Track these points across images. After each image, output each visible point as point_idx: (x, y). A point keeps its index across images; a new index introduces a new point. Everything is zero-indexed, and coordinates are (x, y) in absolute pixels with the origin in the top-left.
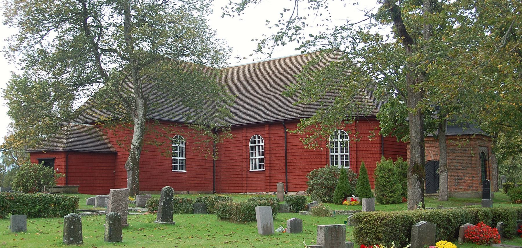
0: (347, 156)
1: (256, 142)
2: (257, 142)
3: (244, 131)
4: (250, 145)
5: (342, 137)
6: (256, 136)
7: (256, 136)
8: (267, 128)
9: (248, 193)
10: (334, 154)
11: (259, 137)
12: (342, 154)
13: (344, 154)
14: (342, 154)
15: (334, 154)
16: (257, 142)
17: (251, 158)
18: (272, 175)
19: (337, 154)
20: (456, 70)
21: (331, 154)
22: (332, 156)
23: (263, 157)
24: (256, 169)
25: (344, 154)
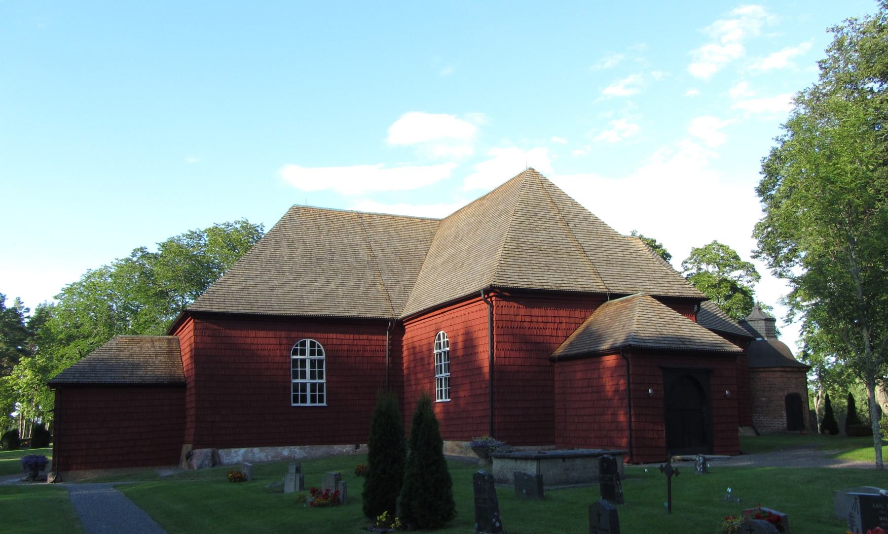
0: (321, 385)
1: (309, 353)
7: (308, 342)
10: (299, 381)
15: (299, 381)
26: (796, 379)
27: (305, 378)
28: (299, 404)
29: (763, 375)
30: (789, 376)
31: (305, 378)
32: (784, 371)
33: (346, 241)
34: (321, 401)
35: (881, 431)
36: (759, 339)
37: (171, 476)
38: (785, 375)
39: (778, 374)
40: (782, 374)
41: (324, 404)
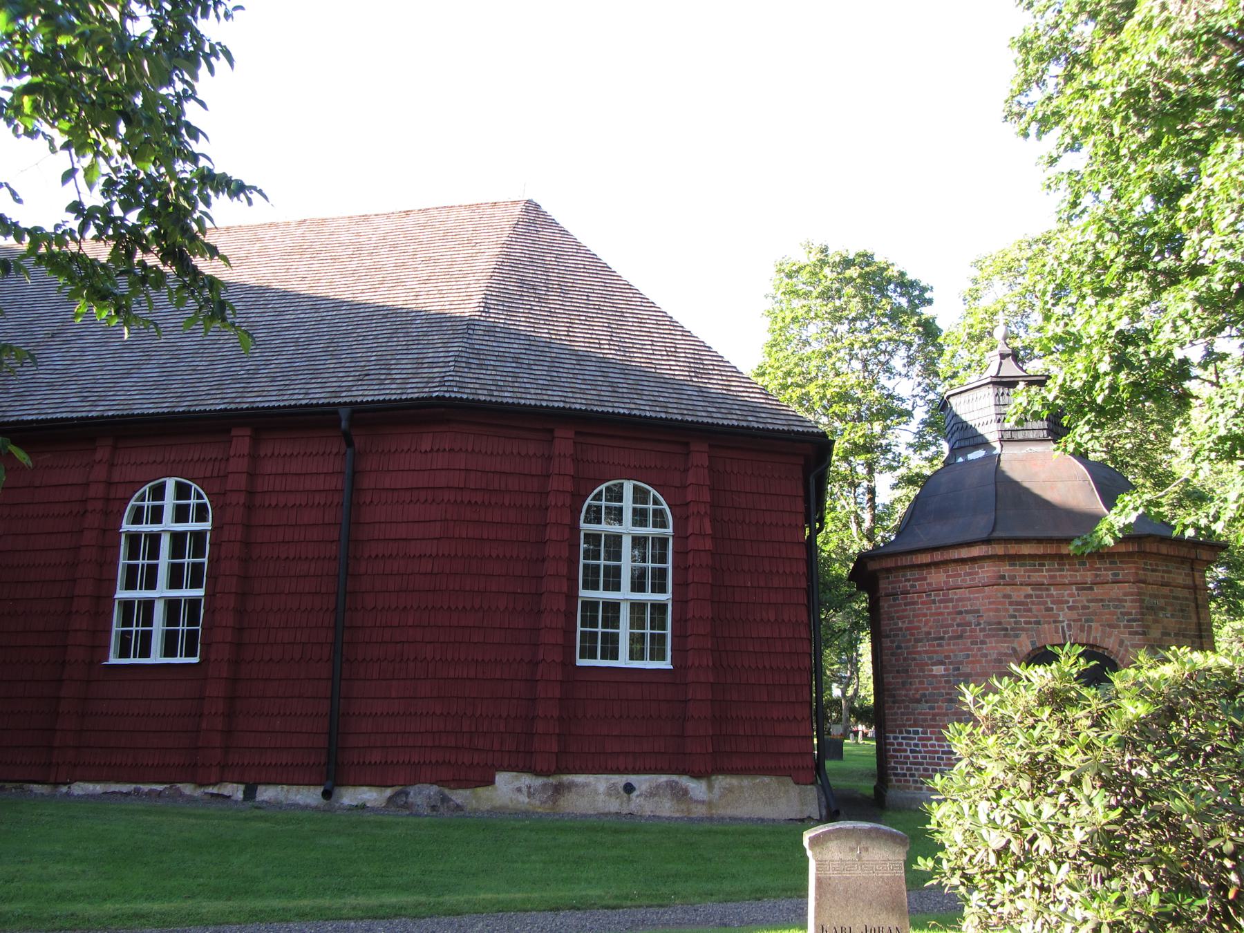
0: (659, 608)
1: (168, 513)
2: (168, 513)
3: (102, 453)
4: (127, 527)
5: (181, 514)
6: (170, 484)
7: (170, 484)
8: (241, 442)
9: (79, 788)
10: (601, 595)
11: (182, 492)
12: (640, 531)
13: (648, 596)
14: (640, 531)
15: (601, 595)
16: (168, 513)
17: (122, 594)
18: (303, 557)
19: (611, 595)
20: (1085, 543)
21: (585, 594)
22: (591, 606)
23: (200, 592)
24: (145, 652)
25: (648, 596)
26: (1083, 587)
27: (617, 587)
28: (599, 662)
29: (937, 578)
30: (1043, 575)
31: (617, 587)
32: (1012, 559)
33: (17, 53)
34: (658, 655)
35: (998, 715)
36: (979, 454)
37: (128, 794)
38: (1020, 572)
39: (986, 572)
40: (1005, 569)
41: (666, 665)
